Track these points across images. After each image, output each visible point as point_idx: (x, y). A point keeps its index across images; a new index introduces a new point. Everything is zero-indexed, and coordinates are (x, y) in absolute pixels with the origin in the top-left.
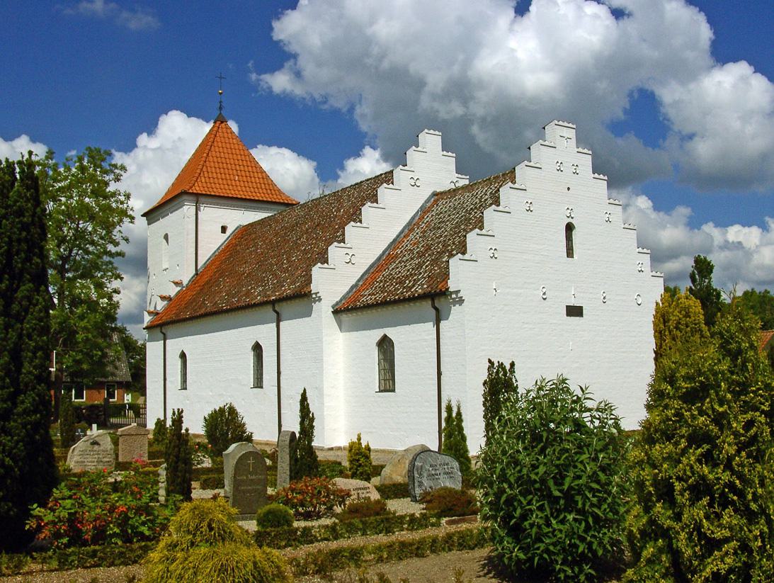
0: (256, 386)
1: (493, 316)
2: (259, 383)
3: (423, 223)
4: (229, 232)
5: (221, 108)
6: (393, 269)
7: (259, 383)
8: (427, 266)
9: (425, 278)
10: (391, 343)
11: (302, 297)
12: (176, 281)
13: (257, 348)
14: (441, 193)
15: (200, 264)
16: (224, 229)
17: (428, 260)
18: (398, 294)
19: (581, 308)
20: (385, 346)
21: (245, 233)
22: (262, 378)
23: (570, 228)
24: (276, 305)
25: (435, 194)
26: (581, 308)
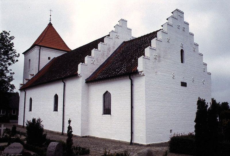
0: (105, 113)
1: (155, 83)
2: (56, 109)
3: (121, 51)
4: (51, 59)
5: (50, 20)
6: (110, 66)
7: (56, 109)
8: (125, 64)
9: (125, 68)
10: (110, 94)
11: (74, 75)
12: (32, 74)
13: (56, 97)
14: (126, 42)
15: (39, 70)
16: (49, 58)
17: (125, 62)
18: (113, 74)
19: (186, 83)
20: (107, 96)
21: (56, 60)
22: (23, 81)
23: (182, 51)
24: (64, 80)
25: (124, 42)
26: (186, 83)
